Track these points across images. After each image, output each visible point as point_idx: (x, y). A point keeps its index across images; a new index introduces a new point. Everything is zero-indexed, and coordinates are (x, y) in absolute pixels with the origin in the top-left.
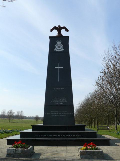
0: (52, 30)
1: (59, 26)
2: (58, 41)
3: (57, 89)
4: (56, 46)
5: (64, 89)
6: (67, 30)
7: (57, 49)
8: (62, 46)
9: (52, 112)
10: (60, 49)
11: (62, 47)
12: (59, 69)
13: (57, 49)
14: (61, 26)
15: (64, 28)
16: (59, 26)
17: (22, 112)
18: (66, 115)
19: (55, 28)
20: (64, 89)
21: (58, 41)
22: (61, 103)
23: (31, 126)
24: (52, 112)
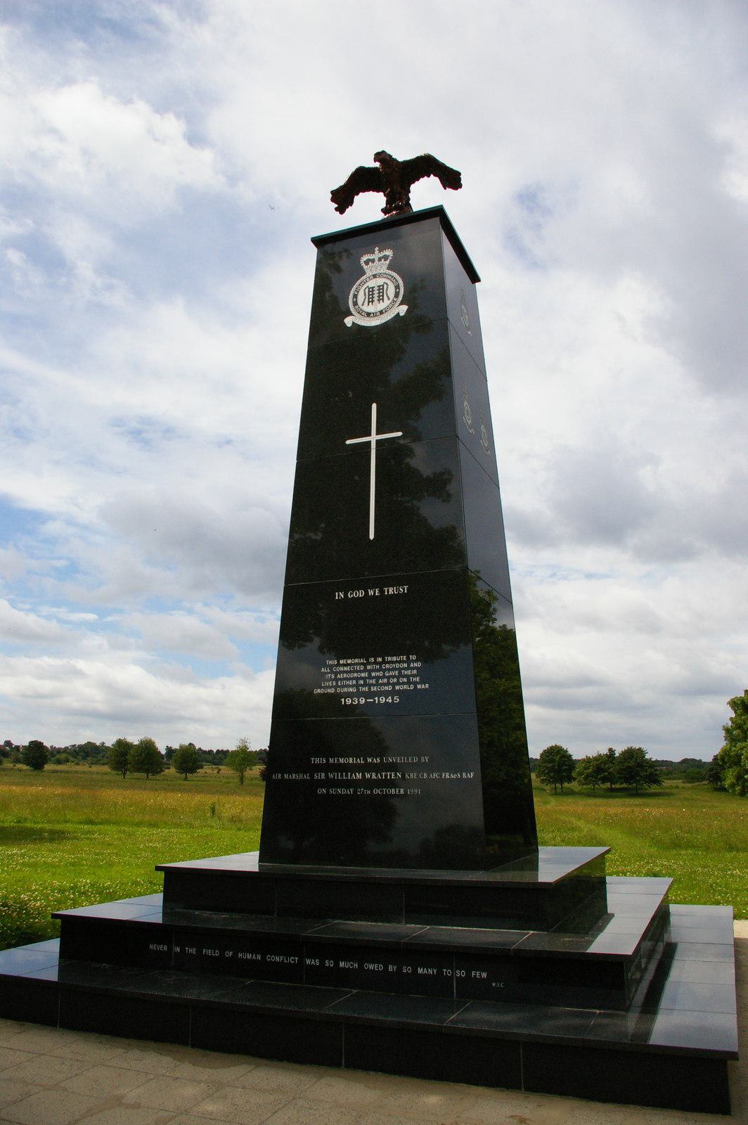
0: (343, 198)
1: (381, 157)
2: (371, 257)
3: (361, 594)
4: (355, 296)
5: (404, 589)
6: (451, 179)
7: (360, 312)
8: (397, 287)
9: (319, 768)
10: (381, 306)
11: (397, 295)
12: (373, 446)
13: (360, 312)
14: (402, 154)
15: (426, 166)
16: (381, 157)
17: (104, 743)
18: (417, 791)
19: (361, 181)
20: (404, 589)
21: (371, 257)
22: (386, 694)
23: (158, 868)
24: (319, 768)
